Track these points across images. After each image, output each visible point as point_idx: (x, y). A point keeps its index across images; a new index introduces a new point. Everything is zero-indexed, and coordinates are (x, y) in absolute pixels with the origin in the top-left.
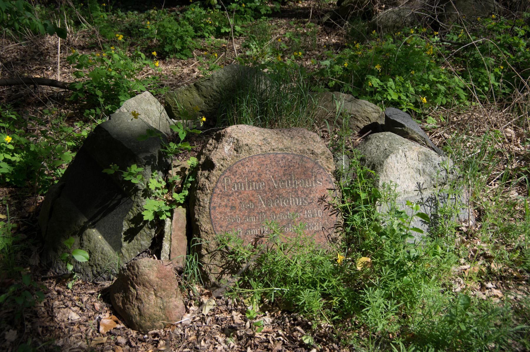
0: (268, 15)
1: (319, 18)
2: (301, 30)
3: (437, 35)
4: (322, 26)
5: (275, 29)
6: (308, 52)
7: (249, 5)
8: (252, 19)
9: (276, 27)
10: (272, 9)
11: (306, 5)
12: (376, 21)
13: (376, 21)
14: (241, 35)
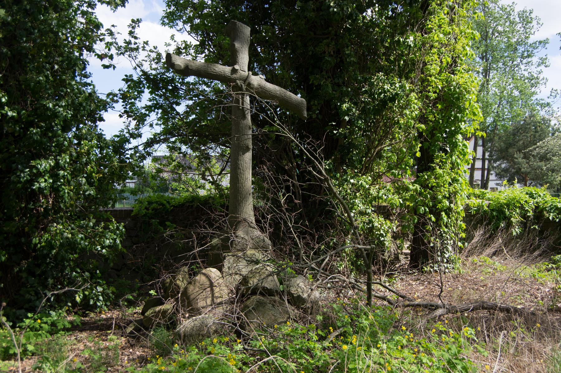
0: (65, 329)
1: (122, 330)
2: (103, 344)
3: (240, 343)
4: (126, 337)
5: (75, 344)
6: (109, 368)
7: (45, 319)
8: (48, 335)
9: (75, 342)
10: (71, 322)
11: (109, 315)
12: (180, 330)
13: (180, 330)
14: (33, 354)
